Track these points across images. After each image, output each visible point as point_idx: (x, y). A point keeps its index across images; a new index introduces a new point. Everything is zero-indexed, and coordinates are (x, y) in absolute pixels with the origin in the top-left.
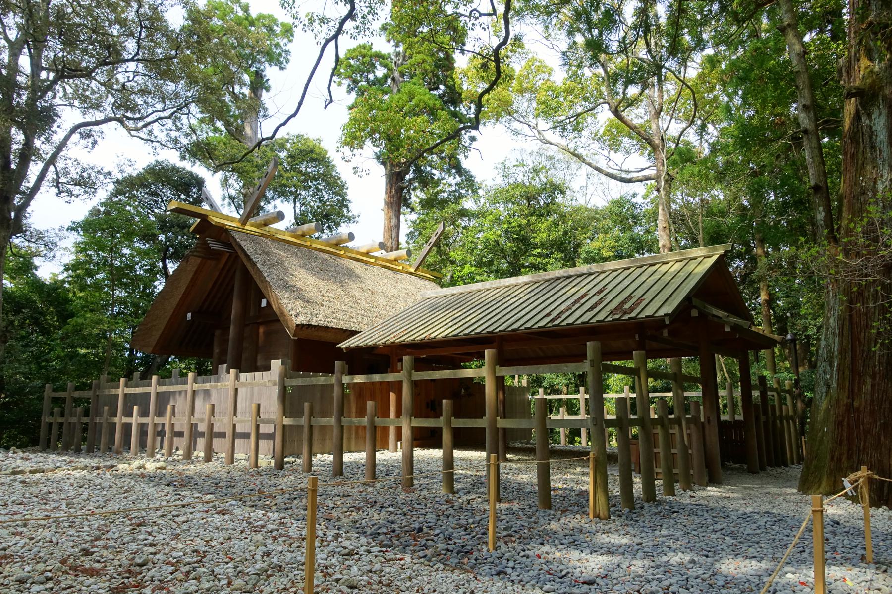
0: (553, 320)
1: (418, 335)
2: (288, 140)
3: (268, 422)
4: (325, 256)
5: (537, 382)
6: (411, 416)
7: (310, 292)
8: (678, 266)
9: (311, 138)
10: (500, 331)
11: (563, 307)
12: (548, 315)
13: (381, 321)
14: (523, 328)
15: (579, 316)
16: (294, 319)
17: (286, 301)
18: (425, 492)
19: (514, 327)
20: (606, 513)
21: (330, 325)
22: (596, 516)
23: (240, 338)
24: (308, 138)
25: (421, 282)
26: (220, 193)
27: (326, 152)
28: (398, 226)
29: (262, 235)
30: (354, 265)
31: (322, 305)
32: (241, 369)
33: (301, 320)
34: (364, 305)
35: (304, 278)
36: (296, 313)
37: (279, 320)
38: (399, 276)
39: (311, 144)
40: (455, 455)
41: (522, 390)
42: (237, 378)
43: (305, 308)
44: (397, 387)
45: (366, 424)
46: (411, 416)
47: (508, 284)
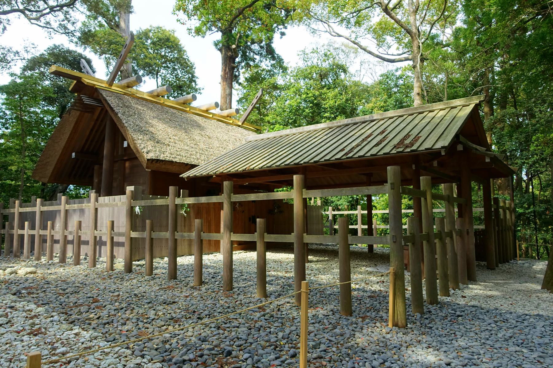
0: (346, 154)
1: (240, 167)
2: (150, 31)
3: (120, 234)
4: (175, 111)
5: (326, 203)
6: (231, 232)
7: (160, 135)
8: (442, 113)
9: (167, 30)
10: (305, 163)
11: (354, 144)
12: (342, 150)
13: (215, 158)
14: (323, 160)
15: (368, 150)
16: (145, 155)
17: (140, 142)
18: (241, 297)
19: (316, 159)
20: (404, 322)
21: (174, 160)
22: (395, 325)
23: (111, 172)
24: (165, 30)
25: (246, 132)
26: (100, 69)
27: (179, 41)
28: (231, 94)
29: (125, 94)
30: (197, 118)
31: (169, 145)
32: (99, 193)
33: (151, 156)
34: (202, 146)
35: (160, 128)
36: (148, 150)
37: (136, 158)
38: (230, 127)
39: (167, 34)
40: (267, 257)
41: (317, 208)
42: (97, 200)
43: (155, 147)
44: (220, 206)
45: (194, 238)
46: (231, 232)
47: (308, 130)
